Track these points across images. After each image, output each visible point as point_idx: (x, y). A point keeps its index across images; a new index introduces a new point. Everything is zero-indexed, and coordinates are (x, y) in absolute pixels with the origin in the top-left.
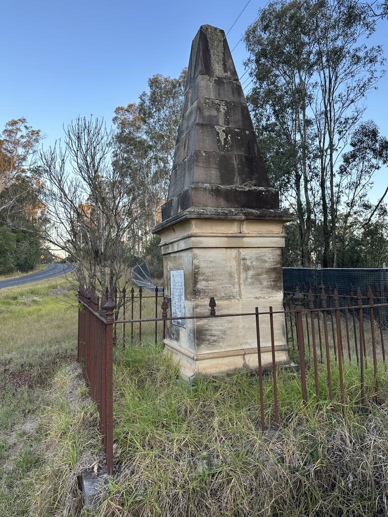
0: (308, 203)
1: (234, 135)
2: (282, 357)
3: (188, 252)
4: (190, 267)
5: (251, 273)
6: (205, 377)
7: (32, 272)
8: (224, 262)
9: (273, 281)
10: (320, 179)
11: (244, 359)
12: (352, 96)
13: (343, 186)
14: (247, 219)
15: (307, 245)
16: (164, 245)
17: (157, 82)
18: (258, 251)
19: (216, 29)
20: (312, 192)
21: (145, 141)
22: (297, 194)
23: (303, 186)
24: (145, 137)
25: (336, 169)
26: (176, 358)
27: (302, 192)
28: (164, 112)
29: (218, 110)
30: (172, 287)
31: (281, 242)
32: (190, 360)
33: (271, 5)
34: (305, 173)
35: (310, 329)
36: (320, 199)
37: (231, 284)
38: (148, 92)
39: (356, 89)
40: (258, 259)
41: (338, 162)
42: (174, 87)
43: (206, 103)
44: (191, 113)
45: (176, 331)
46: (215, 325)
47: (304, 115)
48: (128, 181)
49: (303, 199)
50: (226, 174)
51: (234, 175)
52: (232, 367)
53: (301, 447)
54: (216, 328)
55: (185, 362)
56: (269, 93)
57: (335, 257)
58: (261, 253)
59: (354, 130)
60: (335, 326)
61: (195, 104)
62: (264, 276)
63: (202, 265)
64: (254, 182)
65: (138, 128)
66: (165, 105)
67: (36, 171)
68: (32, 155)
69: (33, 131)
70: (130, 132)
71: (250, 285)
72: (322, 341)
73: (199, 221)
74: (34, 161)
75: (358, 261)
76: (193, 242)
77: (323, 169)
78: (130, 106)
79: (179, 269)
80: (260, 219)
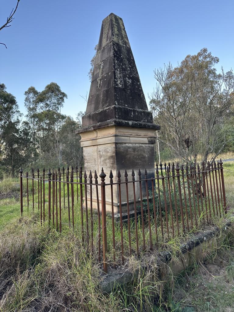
5: (102, 159)
8: (93, 153)
9: (112, 164)
58: (106, 147)
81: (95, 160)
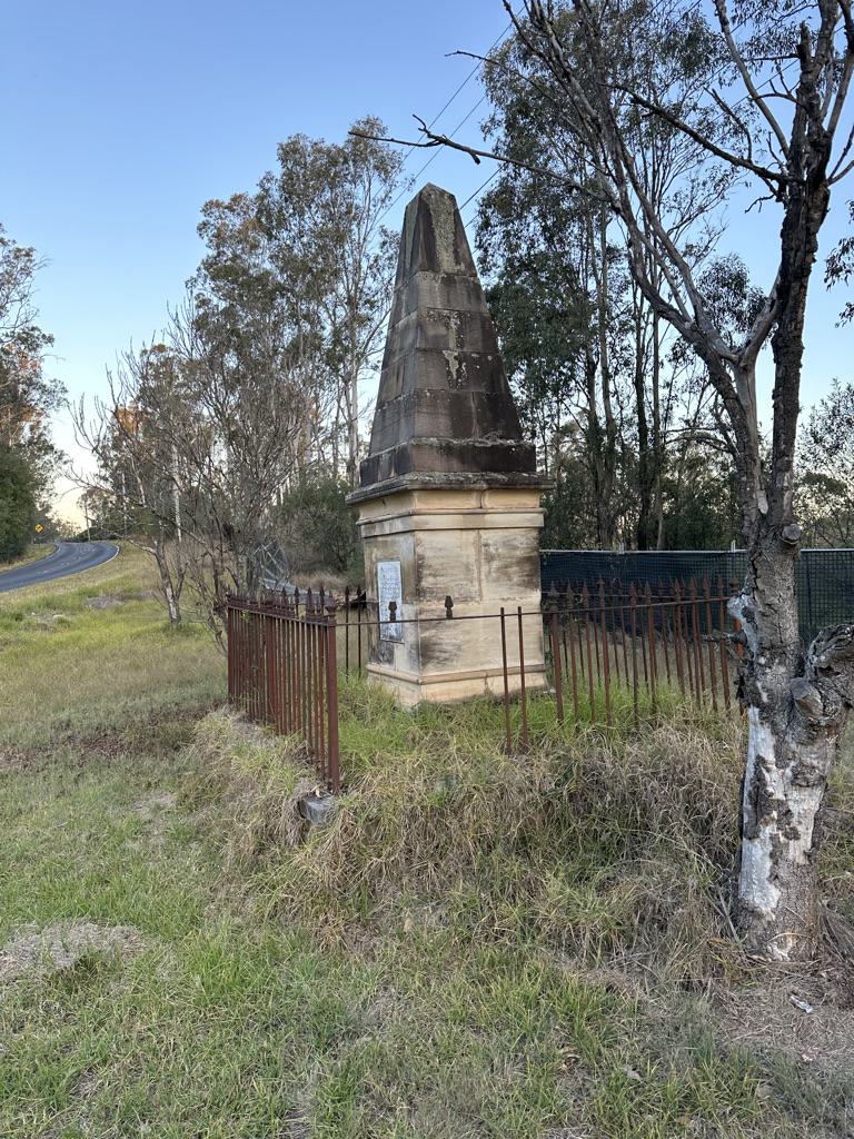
0: (610, 420)
1: (471, 362)
2: (536, 681)
3: (406, 536)
4: (411, 558)
5: (495, 564)
6: (435, 706)
7: (21, 563)
9: (527, 575)
10: (634, 372)
11: (486, 683)
12: (699, 201)
13: (679, 385)
14: (490, 489)
15: (606, 504)
16: (365, 524)
17: (295, 151)
18: (506, 532)
19: (443, 193)
20: (618, 398)
21: (267, 273)
22: (588, 400)
23: (601, 385)
24: (267, 266)
25: (665, 351)
26: (390, 687)
27: (599, 397)
28: (311, 218)
29: (447, 326)
30: (380, 585)
31: (539, 520)
32: (411, 686)
35: (601, 660)
36: (634, 412)
37: (468, 580)
38: (278, 171)
39: (709, 185)
40: (507, 544)
42: (334, 163)
43: (430, 316)
44: (407, 327)
45: (388, 649)
46: (448, 636)
47: (603, 240)
48: (231, 361)
49: (600, 412)
50: (460, 425)
51: (471, 423)
52: (470, 694)
53: (553, 768)
54: (448, 641)
55: (404, 690)
56: (533, 192)
59: (701, 274)
60: (648, 657)
61: (414, 316)
62: (515, 569)
63: (428, 554)
64: (500, 432)
65: (254, 247)
66: (313, 200)
67: (26, 340)
68: (18, 304)
69: (19, 250)
70: (235, 257)
71: (494, 581)
72: (639, 690)
73: (423, 493)
74: (23, 317)
76: (416, 523)
77: (641, 351)
78: (236, 199)
79: (392, 559)
80: (509, 488)
81: (467, 568)
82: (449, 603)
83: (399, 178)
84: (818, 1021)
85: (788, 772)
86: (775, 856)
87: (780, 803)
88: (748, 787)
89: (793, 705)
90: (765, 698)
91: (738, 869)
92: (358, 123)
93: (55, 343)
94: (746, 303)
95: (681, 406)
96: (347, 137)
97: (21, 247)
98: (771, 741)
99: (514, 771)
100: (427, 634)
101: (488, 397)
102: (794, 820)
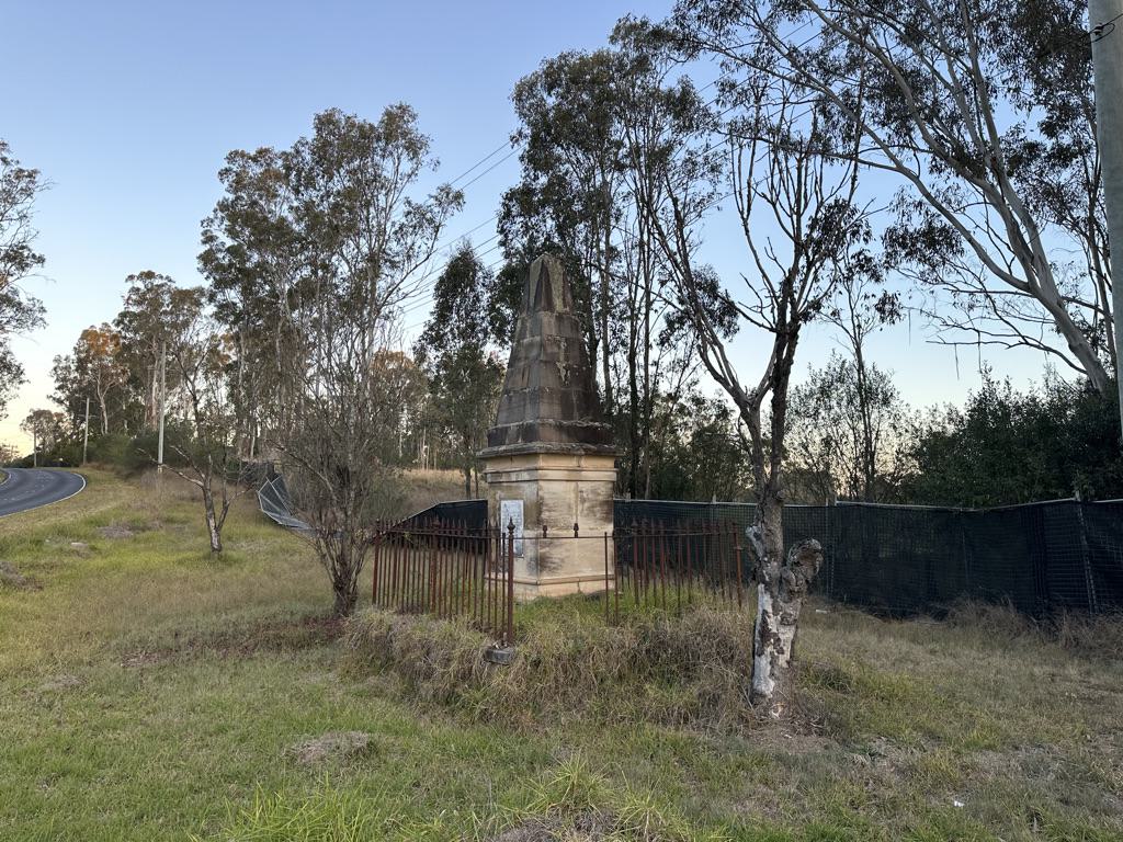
0: (609, 389)
3: (530, 483)
4: (534, 498)
5: (586, 505)
13: (664, 365)
18: (593, 484)
25: (654, 337)
29: (559, 348)
31: (613, 476)
33: (563, 57)
34: (605, 339)
40: (594, 492)
41: (658, 325)
47: (607, 243)
52: (569, 593)
57: (648, 481)
61: (538, 338)
63: (546, 496)
69: (21, 171)
75: (682, 488)
77: (634, 332)
78: (262, 152)
81: (570, 507)
82: (545, 529)
83: (425, 158)
84: (795, 742)
85: (779, 618)
86: (773, 663)
87: (775, 634)
88: (758, 627)
89: (782, 581)
90: (767, 579)
91: (753, 675)
92: (392, 107)
93: (45, 264)
94: (717, 304)
95: (666, 382)
96: (380, 118)
97: (24, 168)
98: (771, 601)
99: (612, 634)
100: (543, 551)
101: (583, 393)
102: (782, 643)
